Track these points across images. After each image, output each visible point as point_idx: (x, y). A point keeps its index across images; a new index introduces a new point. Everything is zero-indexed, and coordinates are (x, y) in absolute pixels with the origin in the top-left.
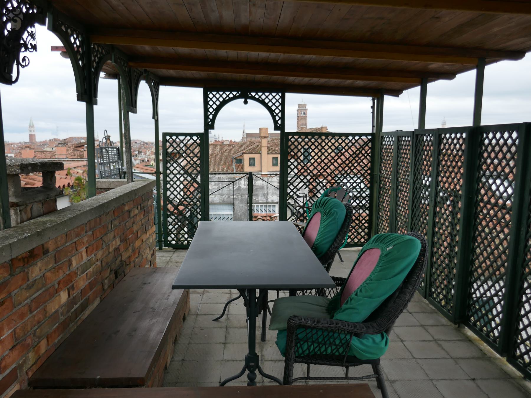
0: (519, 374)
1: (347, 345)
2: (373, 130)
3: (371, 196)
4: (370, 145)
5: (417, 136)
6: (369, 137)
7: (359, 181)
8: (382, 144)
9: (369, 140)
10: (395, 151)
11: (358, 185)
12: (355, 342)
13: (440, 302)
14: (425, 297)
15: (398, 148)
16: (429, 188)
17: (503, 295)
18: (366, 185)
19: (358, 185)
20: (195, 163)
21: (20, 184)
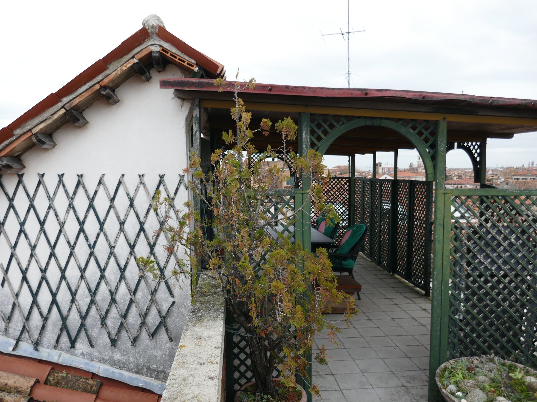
0: (413, 285)
1: (341, 264)
2: (349, 175)
3: (349, 215)
4: (348, 184)
5: (372, 181)
6: (347, 180)
7: (342, 206)
8: (355, 184)
9: (347, 181)
10: (362, 188)
11: (341, 208)
12: (343, 262)
13: (384, 265)
14: (378, 265)
15: (363, 187)
16: (199, 69)
17: (423, 272)
18: (346, 209)
19: (341, 208)
20: (346, 188)
21: (485, 176)
